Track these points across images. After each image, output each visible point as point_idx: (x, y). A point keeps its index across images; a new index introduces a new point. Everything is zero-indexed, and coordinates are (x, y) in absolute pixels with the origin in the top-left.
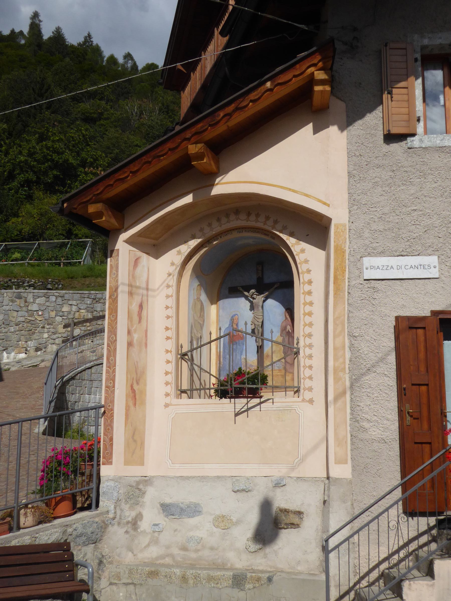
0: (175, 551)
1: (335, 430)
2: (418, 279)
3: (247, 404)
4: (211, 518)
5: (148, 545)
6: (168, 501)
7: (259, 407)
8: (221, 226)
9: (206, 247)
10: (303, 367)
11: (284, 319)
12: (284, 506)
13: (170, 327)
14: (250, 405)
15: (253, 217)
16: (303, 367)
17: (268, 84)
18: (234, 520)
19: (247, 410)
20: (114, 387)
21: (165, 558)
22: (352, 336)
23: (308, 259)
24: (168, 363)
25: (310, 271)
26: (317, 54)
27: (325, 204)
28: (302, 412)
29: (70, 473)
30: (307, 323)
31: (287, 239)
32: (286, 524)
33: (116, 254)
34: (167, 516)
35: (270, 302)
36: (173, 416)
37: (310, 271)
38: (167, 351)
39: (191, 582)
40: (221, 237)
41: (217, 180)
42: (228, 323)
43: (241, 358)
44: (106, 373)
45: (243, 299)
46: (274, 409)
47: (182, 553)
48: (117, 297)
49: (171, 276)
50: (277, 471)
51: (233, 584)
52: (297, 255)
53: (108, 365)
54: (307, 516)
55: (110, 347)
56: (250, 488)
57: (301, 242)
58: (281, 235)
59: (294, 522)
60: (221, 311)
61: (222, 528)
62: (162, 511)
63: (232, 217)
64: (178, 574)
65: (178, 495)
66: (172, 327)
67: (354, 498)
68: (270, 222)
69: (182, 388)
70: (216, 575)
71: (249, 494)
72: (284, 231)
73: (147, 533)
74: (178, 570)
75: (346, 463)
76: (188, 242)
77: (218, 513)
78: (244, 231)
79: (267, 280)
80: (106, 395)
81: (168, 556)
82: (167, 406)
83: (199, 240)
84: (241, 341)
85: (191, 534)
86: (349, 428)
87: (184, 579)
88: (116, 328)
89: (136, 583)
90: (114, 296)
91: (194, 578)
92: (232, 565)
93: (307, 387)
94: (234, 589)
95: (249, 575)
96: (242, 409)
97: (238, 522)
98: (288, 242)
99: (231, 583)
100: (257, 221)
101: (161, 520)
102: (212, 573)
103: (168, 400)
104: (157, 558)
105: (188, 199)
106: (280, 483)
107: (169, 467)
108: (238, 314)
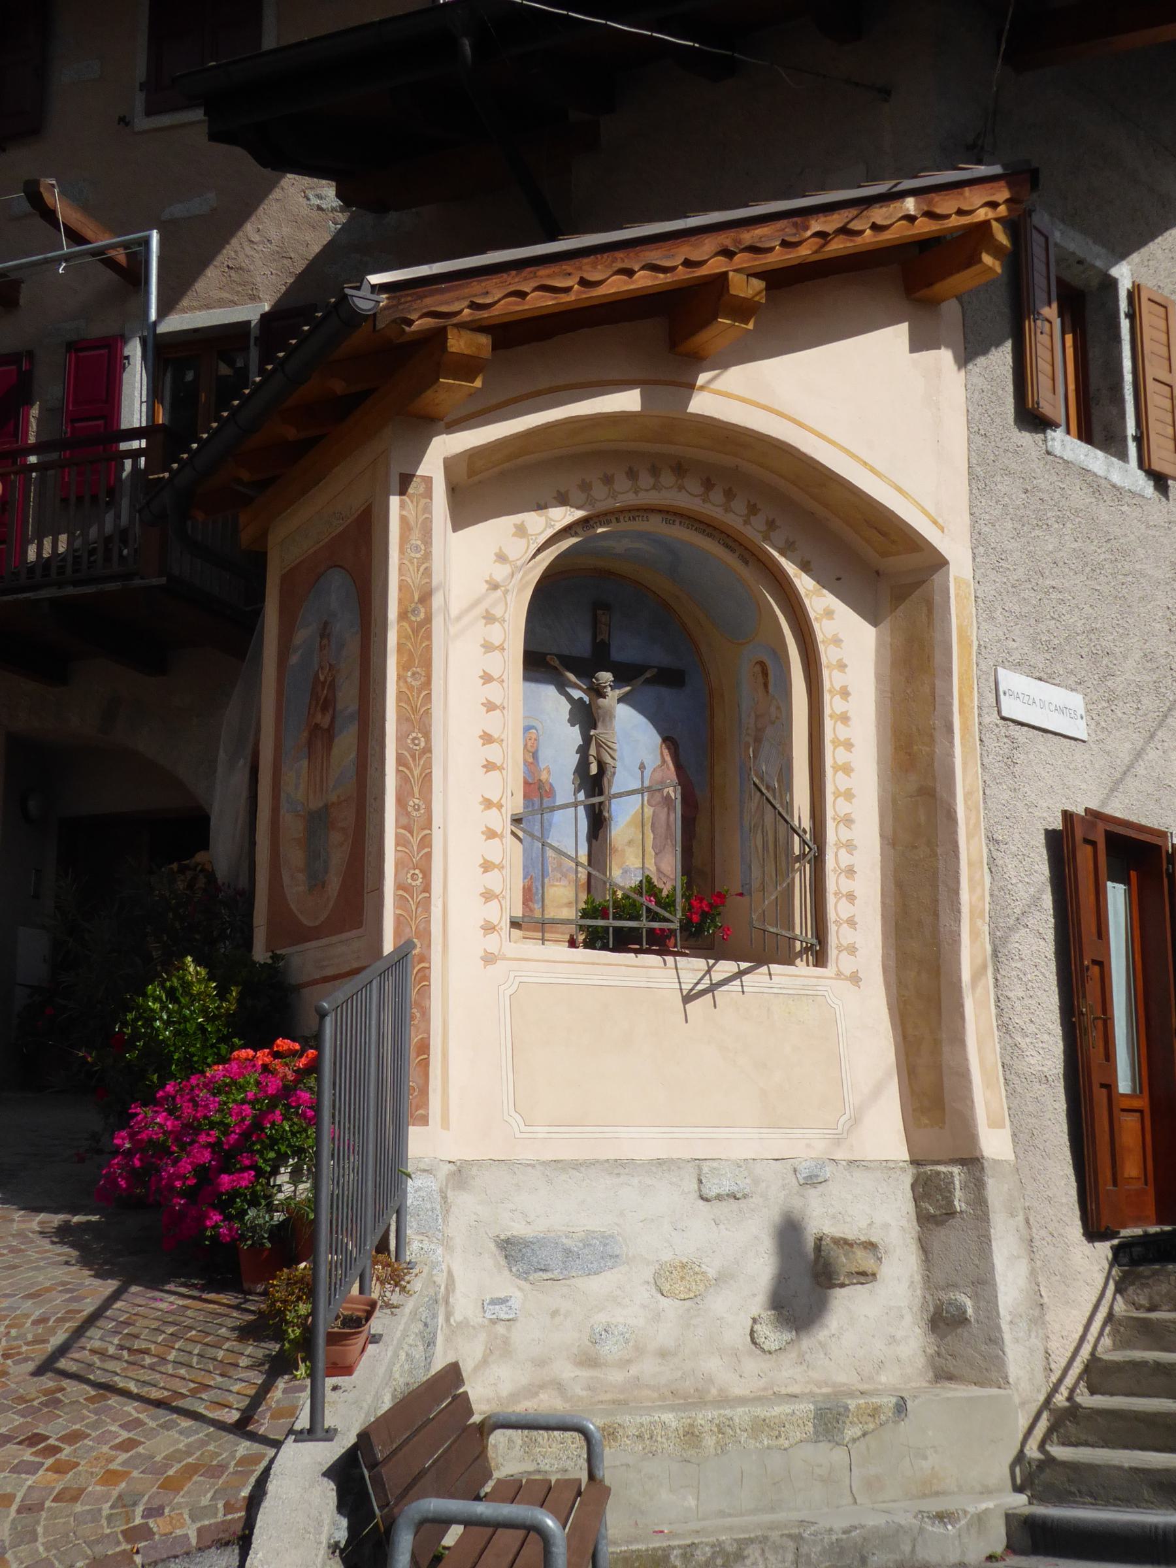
0: (567, 1372)
1: (979, 1050)
2: (1052, 739)
3: (709, 971)
4: (648, 1274)
5: (485, 1362)
6: (519, 1229)
7: (737, 982)
8: (636, 493)
9: (576, 534)
10: (836, 894)
11: (659, 762)
12: (830, 1229)
13: (496, 736)
14: (717, 977)
15: (717, 496)
16: (836, 894)
17: (910, 205)
18: (712, 1273)
19: (712, 988)
20: (427, 888)
21: (537, 1394)
22: (992, 840)
23: (841, 636)
24: (489, 838)
25: (846, 666)
26: (1003, 183)
27: (935, 522)
28: (840, 1003)
30: (842, 789)
31: (796, 576)
32: (850, 1274)
33: (422, 490)
34: (523, 1276)
36: (511, 991)
37: (846, 666)
38: (488, 804)
39: (710, 1441)
40: (618, 520)
41: (703, 378)
44: (397, 844)
46: (776, 991)
47: (585, 1373)
48: (428, 619)
49: (499, 593)
50: (807, 1145)
51: (816, 1433)
52: (816, 619)
53: (404, 821)
54: (886, 1252)
55: (409, 768)
56: (747, 1191)
57: (825, 592)
58: (783, 561)
59: (866, 1269)
61: (682, 1296)
62: (503, 1262)
63: (667, 478)
64: (674, 1425)
65: (541, 1213)
66: (504, 736)
67: (1027, 1204)
68: (759, 522)
69: (546, 916)
70: (774, 1414)
71: (742, 1204)
72: (789, 553)
73: (474, 1328)
74: (671, 1416)
75: (1003, 1127)
76: (546, 507)
77: (666, 1256)
78: (677, 522)
80: (399, 912)
81: (542, 1387)
82: (489, 959)
83: (579, 514)
85: (601, 1318)
86: (998, 1046)
87: (691, 1436)
88: (428, 712)
89: (547, 1468)
90: (416, 615)
91: (716, 1429)
92: (721, 1390)
93: (845, 943)
94: (821, 1444)
95: (852, 1404)
96: (697, 984)
97: (722, 1278)
99: (811, 1430)
100: (727, 510)
101: (505, 1284)
102: (761, 1412)
103: (492, 943)
104: (514, 1397)
105: (628, 401)
106: (817, 1176)
107: (518, 1135)
108: (539, 726)
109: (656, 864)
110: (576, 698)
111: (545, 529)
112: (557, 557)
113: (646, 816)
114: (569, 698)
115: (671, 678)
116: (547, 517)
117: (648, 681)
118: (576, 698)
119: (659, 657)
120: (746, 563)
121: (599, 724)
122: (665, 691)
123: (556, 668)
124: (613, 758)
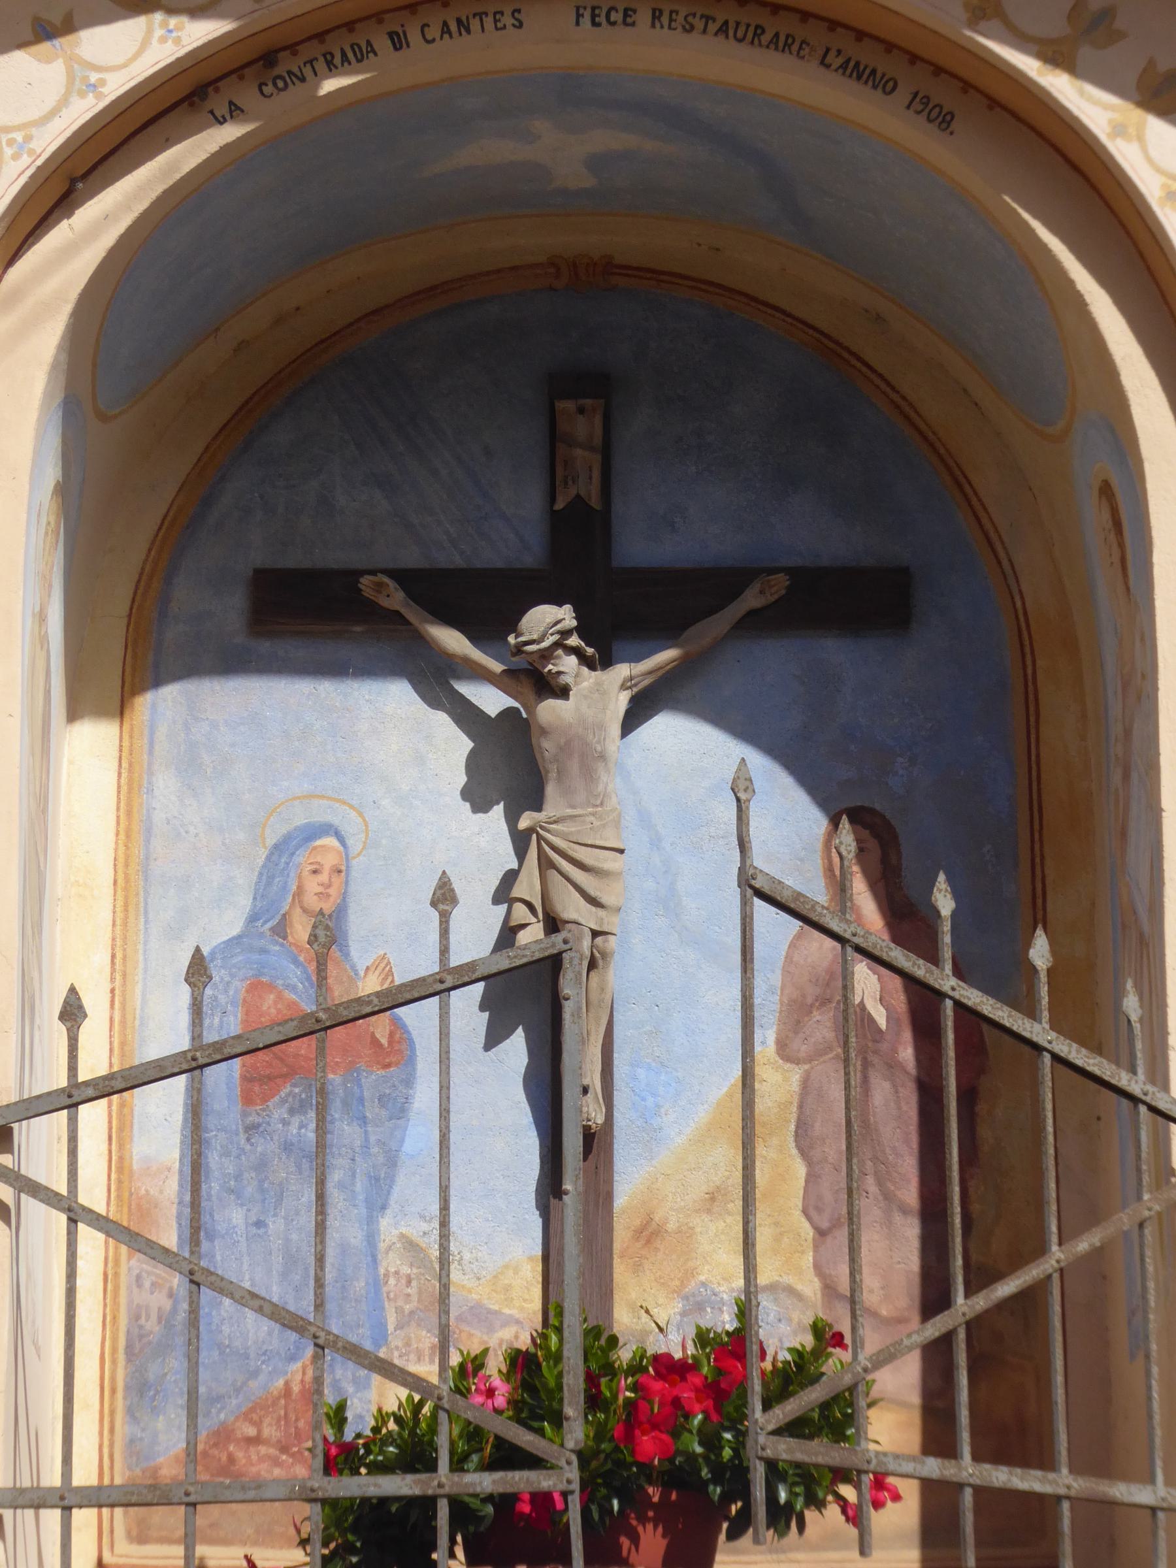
9: (235, 112)
29: (823, 1422)
31: (1119, 130)
35: (673, 734)
40: (398, 41)
42: (244, 902)
43: (371, 1239)
45: (396, 698)
60: (165, 785)
72: (1086, 53)
76: (68, 26)
79: (639, 544)
83: (199, 32)
84: (371, 1079)
98: (1128, 156)
108: (350, 823)
109: (817, 1267)
110: (492, 710)
111: (64, 102)
112: (165, 192)
113: (764, 1105)
114: (467, 716)
115: (855, 601)
116: (72, 61)
117: (755, 624)
118: (492, 710)
119: (812, 533)
120: (944, 120)
121: (551, 790)
122: (834, 650)
123: (397, 617)
124: (594, 902)
